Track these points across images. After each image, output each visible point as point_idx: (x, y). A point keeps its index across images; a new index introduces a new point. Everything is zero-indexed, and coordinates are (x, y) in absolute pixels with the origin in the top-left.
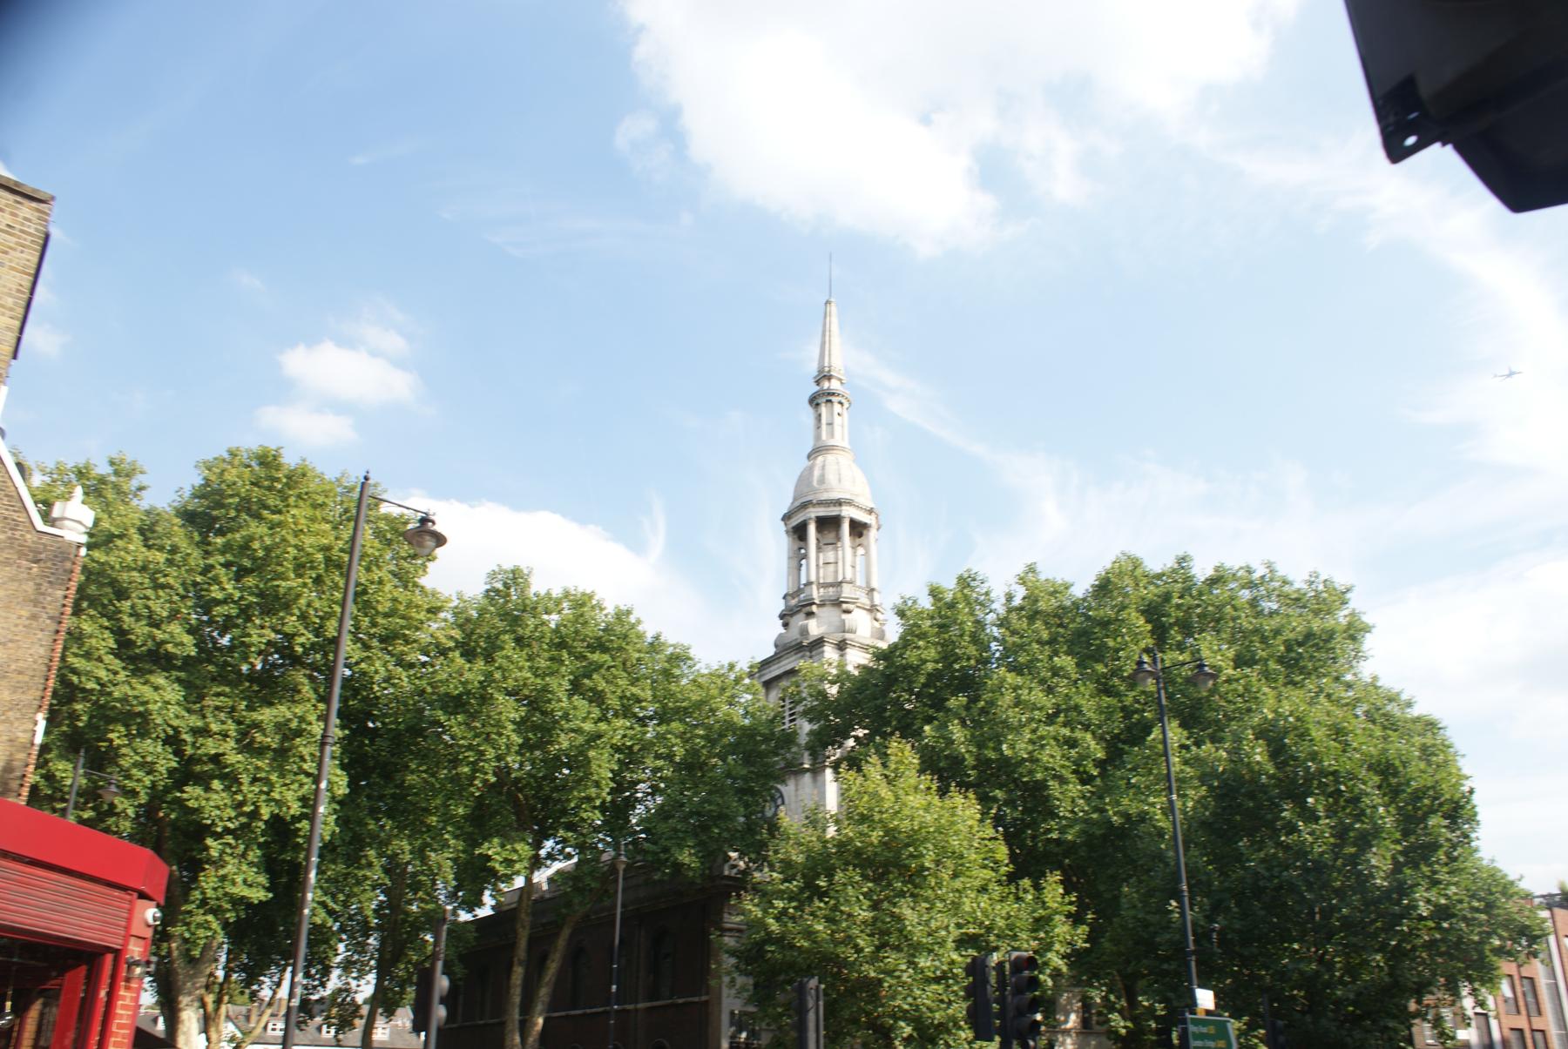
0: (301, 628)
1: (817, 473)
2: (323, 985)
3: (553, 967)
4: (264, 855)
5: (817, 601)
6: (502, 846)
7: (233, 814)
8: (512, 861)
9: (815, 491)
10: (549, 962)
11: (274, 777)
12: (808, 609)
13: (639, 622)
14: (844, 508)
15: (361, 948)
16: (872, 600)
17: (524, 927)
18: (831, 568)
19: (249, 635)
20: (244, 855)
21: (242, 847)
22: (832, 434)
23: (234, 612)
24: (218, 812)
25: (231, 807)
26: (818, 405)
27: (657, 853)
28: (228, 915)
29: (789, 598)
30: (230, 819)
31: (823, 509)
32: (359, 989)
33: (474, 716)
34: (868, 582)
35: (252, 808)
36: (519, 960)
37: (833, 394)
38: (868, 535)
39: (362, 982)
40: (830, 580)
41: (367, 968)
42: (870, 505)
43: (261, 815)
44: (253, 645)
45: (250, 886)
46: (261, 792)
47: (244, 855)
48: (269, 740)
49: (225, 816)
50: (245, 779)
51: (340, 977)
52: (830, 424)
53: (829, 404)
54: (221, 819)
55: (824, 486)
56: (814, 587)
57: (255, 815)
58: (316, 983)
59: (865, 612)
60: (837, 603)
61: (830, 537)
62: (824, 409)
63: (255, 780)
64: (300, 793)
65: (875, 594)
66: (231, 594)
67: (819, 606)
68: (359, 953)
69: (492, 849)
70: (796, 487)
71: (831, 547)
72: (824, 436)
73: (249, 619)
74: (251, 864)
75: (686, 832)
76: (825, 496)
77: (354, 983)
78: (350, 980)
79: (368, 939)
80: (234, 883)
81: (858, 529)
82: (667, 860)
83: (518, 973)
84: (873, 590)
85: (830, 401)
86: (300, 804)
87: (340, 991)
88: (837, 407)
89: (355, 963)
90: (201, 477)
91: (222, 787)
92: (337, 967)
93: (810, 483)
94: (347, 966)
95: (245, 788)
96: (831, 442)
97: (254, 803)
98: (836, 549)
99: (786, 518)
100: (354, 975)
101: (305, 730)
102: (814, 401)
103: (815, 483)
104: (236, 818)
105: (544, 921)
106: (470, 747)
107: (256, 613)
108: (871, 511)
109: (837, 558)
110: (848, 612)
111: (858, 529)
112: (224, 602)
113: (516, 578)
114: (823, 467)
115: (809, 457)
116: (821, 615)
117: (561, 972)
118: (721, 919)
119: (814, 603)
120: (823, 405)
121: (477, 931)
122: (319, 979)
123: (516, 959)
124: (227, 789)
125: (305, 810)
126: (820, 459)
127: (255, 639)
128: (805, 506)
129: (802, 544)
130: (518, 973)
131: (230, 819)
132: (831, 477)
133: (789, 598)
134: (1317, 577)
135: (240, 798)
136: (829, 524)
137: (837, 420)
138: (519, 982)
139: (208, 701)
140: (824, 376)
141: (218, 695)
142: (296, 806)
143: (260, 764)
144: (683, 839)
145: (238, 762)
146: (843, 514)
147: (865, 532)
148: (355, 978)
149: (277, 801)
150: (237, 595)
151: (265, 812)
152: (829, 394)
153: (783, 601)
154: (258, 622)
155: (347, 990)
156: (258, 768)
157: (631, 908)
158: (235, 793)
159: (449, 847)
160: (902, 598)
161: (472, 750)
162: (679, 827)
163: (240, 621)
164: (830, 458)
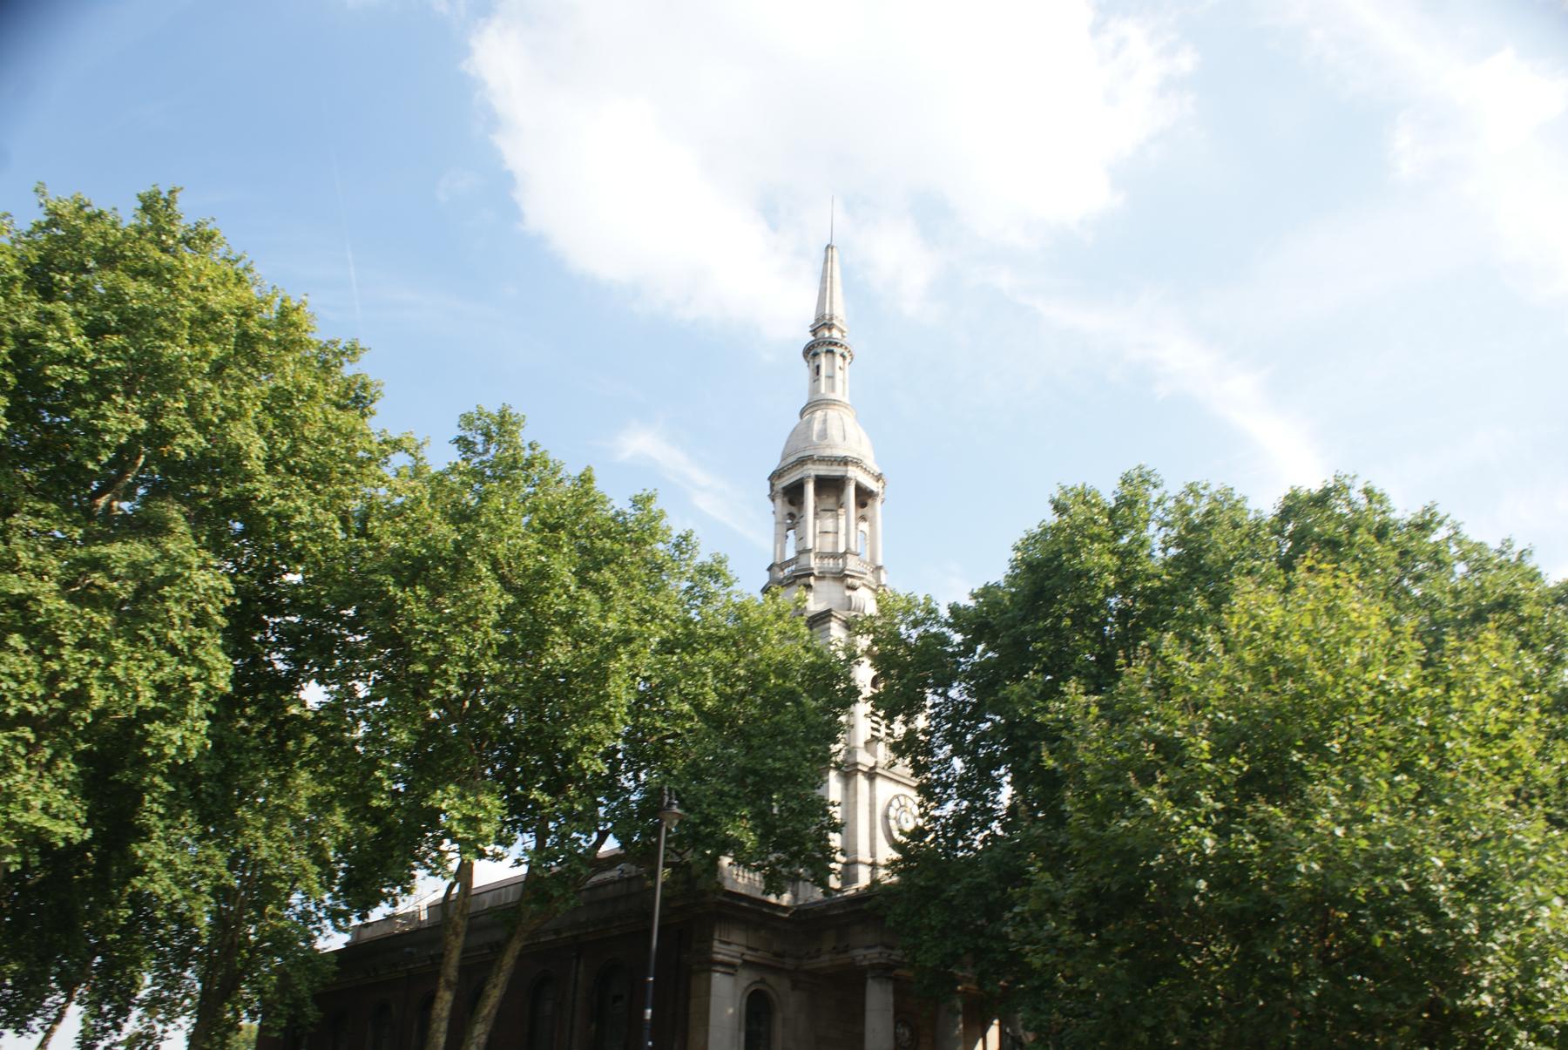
0: (186, 425)
1: (817, 427)
2: (118, 1028)
3: (494, 996)
4: (81, 774)
5: (816, 572)
6: (462, 797)
7: (40, 692)
8: (476, 820)
9: (816, 447)
10: (488, 988)
11: (118, 644)
12: (804, 580)
13: (662, 514)
14: (850, 468)
15: (173, 983)
16: (878, 579)
17: (457, 935)
18: (830, 538)
19: (104, 417)
20: (49, 765)
21: (48, 752)
22: (833, 389)
23: (82, 378)
24: (13, 685)
25: (37, 679)
26: (816, 355)
27: (694, 825)
28: (8, 859)
29: (776, 569)
30: (33, 699)
31: (825, 467)
32: (166, 1035)
33: (437, 590)
34: (873, 559)
35: (75, 685)
36: (447, 982)
37: (836, 344)
38: (873, 507)
39: (171, 1027)
40: (829, 549)
41: (179, 1009)
42: (878, 471)
43: (90, 698)
44: (109, 431)
45: (55, 817)
46: (93, 664)
47: (49, 765)
48: (115, 585)
49: (26, 690)
50: (68, 638)
51: (140, 1019)
52: (831, 377)
53: (830, 355)
54: (18, 696)
55: (826, 442)
56: (812, 555)
57: (79, 697)
58: (108, 1024)
59: (869, 592)
60: (841, 576)
61: (830, 502)
62: (823, 360)
63: (82, 645)
64: (158, 676)
65: (882, 572)
66: (81, 351)
67: (817, 578)
68: (171, 989)
69: (447, 800)
70: (788, 442)
71: (830, 514)
72: (823, 390)
73: (106, 395)
74: (61, 784)
75: (736, 797)
76: (827, 452)
77: (159, 1028)
78: (154, 1022)
79: (185, 970)
80: (26, 807)
81: (864, 496)
82: (711, 835)
83: (445, 1002)
84: (879, 568)
85: (832, 352)
86: (154, 694)
87: (139, 1036)
88: (839, 360)
89: (163, 1001)
90: (44, 209)
91: (25, 647)
92: (139, 1006)
93: (808, 438)
94: (151, 1005)
95: (66, 653)
96: (832, 396)
97: (78, 680)
98: (837, 517)
99: (775, 476)
100: (161, 1017)
101: (180, 575)
102: (811, 352)
103: (814, 438)
104: (44, 698)
105: (432, 952)
106: (434, 637)
107: (119, 388)
108: (878, 478)
109: (837, 527)
110: (853, 588)
111: (864, 496)
112: (68, 361)
113: (502, 426)
114: (825, 421)
115: (802, 414)
116: (819, 589)
117: (504, 1000)
118: (711, 947)
119: (812, 574)
120: (823, 355)
121: (337, 964)
122: (113, 1020)
123: (442, 980)
124: (36, 651)
125: (160, 704)
126: (819, 414)
127: (113, 424)
128: (802, 462)
129: (794, 510)
130: (445, 1002)
131: (33, 699)
132: (834, 433)
133: (776, 569)
134: (1510, 547)
135: (55, 666)
136: (831, 487)
137: (839, 374)
138: (445, 1014)
139: (17, 520)
140: (823, 323)
141: (36, 514)
142: (148, 694)
143: (96, 617)
144: (732, 808)
145: (60, 611)
146: (850, 474)
147: (870, 502)
148: (160, 1021)
149: (118, 684)
150: (91, 356)
151: (98, 696)
152: (830, 343)
153: (767, 574)
154: (120, 400)
155: (150, 1037)
156: (91, 625)
157: (564, 935)
158: (49, 658)
159: (382, 790)
160: (1062, 488)
161: (434, 641)
162: (726, 789)
163: (90, 397)
164: (832, 413)
